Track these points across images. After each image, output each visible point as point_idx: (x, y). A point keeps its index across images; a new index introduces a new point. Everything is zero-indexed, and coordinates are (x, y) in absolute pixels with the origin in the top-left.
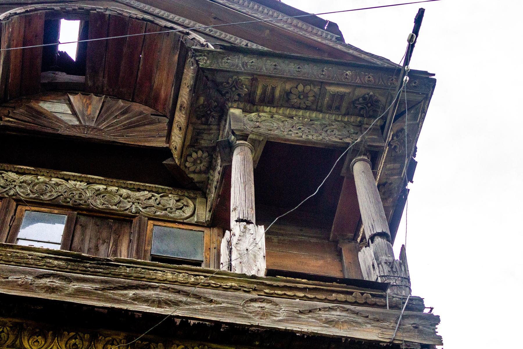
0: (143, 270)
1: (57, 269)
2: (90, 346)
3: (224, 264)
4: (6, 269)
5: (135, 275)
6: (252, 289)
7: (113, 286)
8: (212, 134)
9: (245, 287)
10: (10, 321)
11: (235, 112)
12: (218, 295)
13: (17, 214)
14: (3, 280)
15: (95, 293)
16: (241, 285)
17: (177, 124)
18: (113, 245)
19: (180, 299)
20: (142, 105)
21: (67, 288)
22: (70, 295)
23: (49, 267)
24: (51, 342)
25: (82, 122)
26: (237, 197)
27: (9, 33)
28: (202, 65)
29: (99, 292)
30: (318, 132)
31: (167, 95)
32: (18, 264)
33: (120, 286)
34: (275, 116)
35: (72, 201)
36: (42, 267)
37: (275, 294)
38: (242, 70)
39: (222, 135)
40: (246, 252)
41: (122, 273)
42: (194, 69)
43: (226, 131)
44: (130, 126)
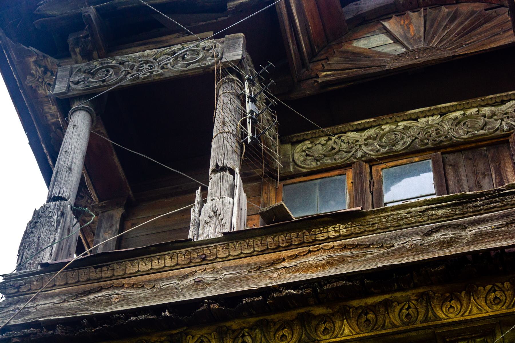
1: (444, 219)
4: (388, 237)
10: (413, 294)
14: (389, 250)
15: (499, 232)
18: (496, 176)
20: (469, 3)
21: (464, 237)
22: (470, 243)
23: (434, 219)
24: (467, 304)
25: (409, 46)
29: (503, 229)
32: (399, 227)
35: (431, 141)
36: (426, 223)
44: (466, 32)
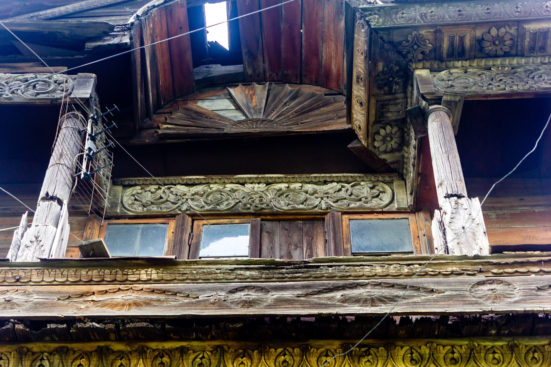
0: (348, 268)
2: (302, 361)
3: (439, 248)
4: (195, 288)
5: (339, 274)
6: (477, 271)
7: (316, 290)
8: (399, 103)
9: (469, 270)
10: (209, 345)
11: (421, 73)
12: (438, 283)
13: (194, 230)
14: (194, 300)
16: (464, 269)
17: (356, 99)
18: (307, 249)
19: (396, 294)
21: (265, 300)
22: (269, 307)
23: (241, 279)
24: (257, 363)
25: (249, 115)
26: (441, 170)
27: (150, 29)
28: (373, 25)
30: (523, 81)
31: (338, 70)
32: (207, 281)
33: (325, 289)
34: (469, 70)
37: (505, 273)
38: (421, 22)
39: (411, 103)
40: (463, 231)
41: (324, 275)
42: (365, 32)
43: (415, 98)
